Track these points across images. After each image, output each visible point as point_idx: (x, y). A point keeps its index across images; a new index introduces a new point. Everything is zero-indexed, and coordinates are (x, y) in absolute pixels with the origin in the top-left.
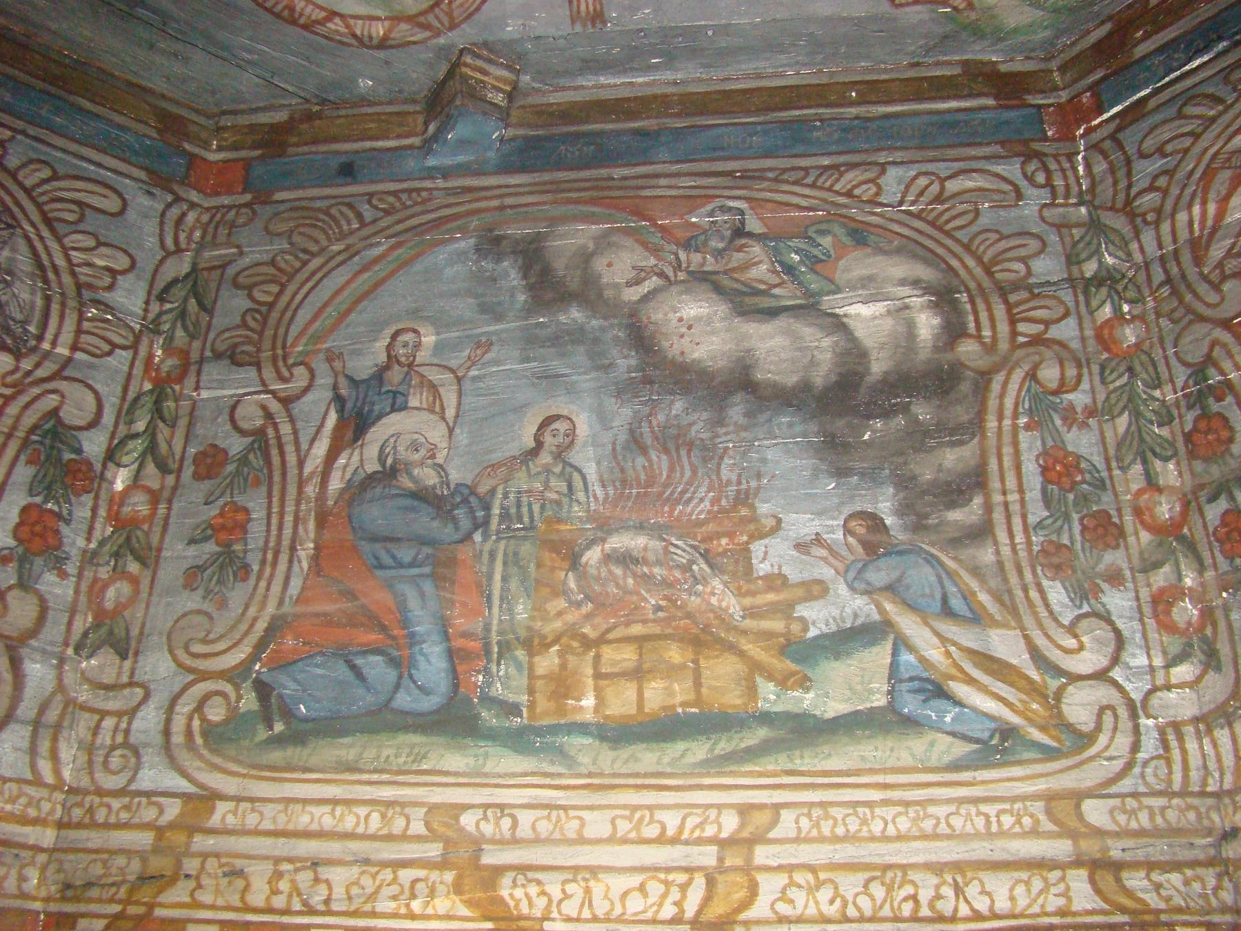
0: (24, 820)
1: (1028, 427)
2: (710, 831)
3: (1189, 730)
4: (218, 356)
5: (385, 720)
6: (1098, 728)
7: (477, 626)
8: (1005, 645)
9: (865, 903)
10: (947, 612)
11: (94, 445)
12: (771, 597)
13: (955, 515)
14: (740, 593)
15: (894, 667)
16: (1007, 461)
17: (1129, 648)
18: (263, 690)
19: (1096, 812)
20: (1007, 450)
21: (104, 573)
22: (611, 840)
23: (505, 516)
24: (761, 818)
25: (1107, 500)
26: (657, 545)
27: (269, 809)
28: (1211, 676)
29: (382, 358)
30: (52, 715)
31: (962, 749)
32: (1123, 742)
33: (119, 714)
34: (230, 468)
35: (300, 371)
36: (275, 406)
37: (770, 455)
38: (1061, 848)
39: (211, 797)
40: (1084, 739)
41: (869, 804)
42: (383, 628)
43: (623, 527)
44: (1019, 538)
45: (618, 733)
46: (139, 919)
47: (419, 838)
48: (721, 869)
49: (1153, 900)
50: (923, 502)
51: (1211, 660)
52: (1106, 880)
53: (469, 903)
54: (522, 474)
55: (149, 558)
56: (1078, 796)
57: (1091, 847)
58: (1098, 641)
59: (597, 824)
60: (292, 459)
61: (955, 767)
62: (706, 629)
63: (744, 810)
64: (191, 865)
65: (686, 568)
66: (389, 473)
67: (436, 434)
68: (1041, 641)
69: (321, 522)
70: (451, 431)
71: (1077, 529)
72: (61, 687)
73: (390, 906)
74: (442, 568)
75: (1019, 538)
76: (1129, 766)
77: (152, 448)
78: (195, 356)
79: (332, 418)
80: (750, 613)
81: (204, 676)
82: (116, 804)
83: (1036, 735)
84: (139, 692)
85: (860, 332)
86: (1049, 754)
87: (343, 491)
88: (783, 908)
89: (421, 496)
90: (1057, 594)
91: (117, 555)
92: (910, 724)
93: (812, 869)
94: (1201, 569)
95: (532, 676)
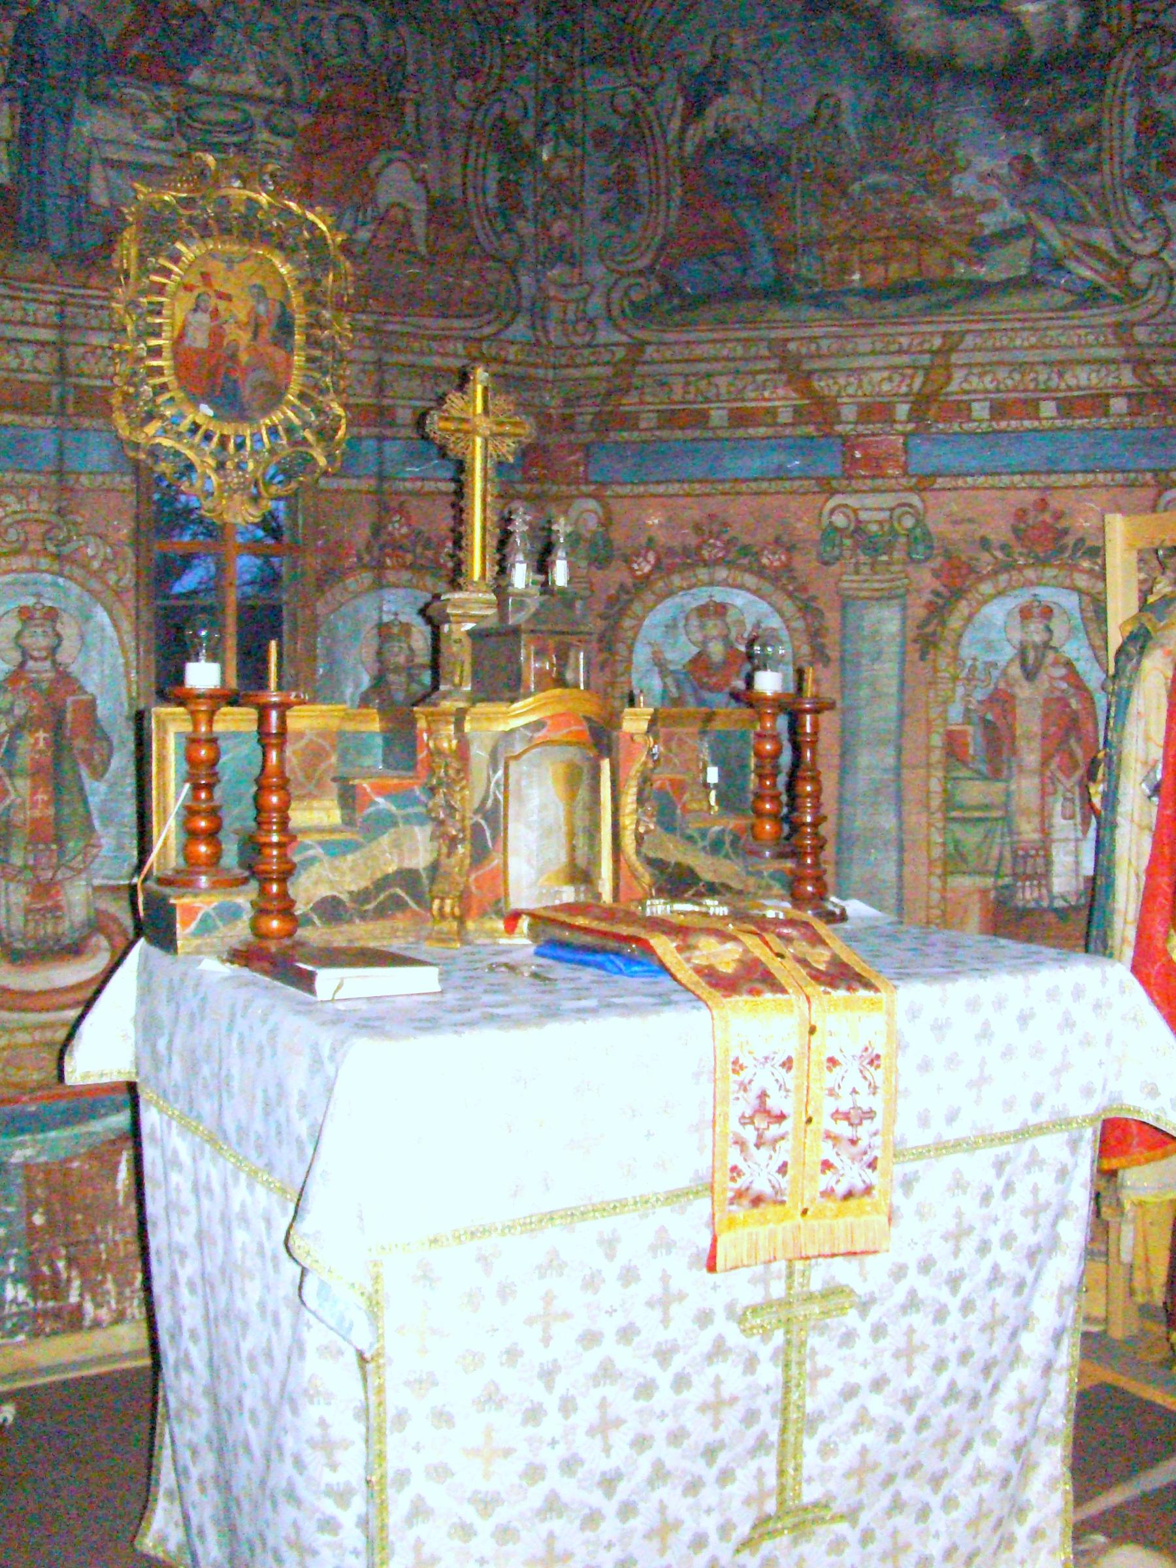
0: (536, 366)
2: (926, 346)
4: (593, 60)
5: (733, 294)
6: (1149, 285)
8: (1100, 238)
10: (1068, 218)
11: (527, 132)
13: (1079, 156)
15: (1034, 251)
18: (665, 282)
19: (1141, 334)
20: (1116, 110)
22: (873, 352)
24: (955, 338)
29: (708, 58)
31: (1068, 298)
32: (1162, 294)
33: (577, 301)
35: (653, 71)
36: (640, 95)
39: (641, 345)
45: (873, 294)
48: (932, 367)
59: (864, 345)
60: (657, 131)
61: (1065, 308)
63: (945, 335)
64: (637, 382)
66: (724, 139)
73: (753, 395)
75: (1117, 171)
76: (1163, 309)
78: (577, 59)
79: (680, 102)
81: (623, 275)
82: (586, 352)
84: (587, 288)
85: (1028, 24)
86: (1119, 301)
88: (966, 386)
89: (746, 152)
90: (1135, 206)
93: (982, 365)
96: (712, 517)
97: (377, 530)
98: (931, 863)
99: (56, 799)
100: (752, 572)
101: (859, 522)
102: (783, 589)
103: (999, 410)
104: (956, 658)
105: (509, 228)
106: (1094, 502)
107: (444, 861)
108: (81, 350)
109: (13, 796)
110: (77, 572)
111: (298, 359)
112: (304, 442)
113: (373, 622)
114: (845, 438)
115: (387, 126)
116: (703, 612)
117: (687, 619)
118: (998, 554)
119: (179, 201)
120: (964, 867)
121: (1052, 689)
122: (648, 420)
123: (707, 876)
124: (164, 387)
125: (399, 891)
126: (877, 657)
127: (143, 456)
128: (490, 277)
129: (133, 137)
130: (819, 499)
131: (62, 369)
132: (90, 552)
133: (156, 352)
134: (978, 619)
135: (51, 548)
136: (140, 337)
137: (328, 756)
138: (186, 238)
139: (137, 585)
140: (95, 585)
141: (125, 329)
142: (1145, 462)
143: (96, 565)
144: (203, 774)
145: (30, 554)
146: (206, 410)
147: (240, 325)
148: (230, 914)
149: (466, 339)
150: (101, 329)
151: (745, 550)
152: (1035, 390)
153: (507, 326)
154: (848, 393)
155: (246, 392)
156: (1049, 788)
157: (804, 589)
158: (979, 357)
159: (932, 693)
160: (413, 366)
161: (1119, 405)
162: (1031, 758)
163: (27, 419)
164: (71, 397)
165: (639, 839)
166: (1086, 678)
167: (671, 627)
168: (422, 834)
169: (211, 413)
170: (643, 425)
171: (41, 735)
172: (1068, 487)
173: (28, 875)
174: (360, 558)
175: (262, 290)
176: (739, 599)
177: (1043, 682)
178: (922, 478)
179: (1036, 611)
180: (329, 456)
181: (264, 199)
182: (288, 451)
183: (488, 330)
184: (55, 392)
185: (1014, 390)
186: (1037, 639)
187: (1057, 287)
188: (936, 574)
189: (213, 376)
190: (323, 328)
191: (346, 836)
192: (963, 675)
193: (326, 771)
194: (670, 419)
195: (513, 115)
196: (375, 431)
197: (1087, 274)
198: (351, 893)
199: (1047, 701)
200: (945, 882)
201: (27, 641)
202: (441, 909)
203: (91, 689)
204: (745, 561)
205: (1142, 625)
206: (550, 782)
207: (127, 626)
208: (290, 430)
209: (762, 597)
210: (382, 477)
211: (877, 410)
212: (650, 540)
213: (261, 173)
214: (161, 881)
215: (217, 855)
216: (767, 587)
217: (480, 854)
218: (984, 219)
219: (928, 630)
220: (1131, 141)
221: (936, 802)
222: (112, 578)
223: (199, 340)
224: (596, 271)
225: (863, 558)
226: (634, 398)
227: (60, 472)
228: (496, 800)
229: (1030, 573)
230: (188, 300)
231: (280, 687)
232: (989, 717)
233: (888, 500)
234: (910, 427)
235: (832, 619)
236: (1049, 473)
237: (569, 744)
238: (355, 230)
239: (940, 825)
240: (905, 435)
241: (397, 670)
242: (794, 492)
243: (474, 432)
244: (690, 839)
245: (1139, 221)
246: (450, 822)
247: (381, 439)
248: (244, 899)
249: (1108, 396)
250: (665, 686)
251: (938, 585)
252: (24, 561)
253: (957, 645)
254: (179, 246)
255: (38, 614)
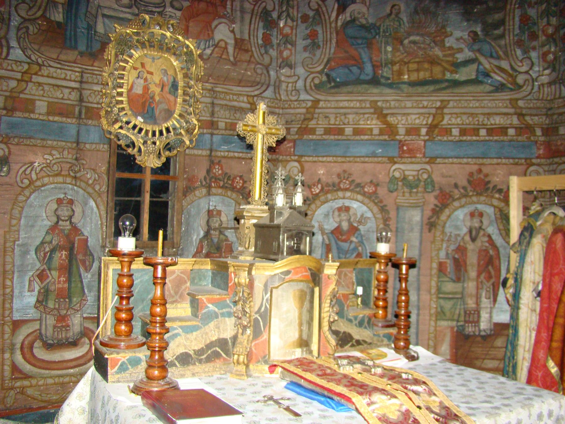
0: (275, 108)
1: (518, 8)
2: (434, 106)
3: (546, 86)
5: (358, 82)
6: (524, 85)
7: (379, 59)
8: (505, 64)
9: (467, 121)
10: (491, 56)
12: (449, 52)
14: (442, 51)
15: (477, 70)
16: (511, 17)
17: (535, 66)
18: (328, 75)
19: (521, 103)
20: (511, 14)
21: (282, 48)
22: (412, 107)
23: (384, 32)
24: (446, 103)
25: (535, 28)
26: (422, 39)
27: (333, 103)
28: (554, 73)
30: (277, 84)
31: (492, 88)
32: (530, 88)
33: (293, 83)
34: (311, 20)
37: (450, 15)
38: (512, 111)
39: (318, 101)
40: (520, 87)
41: (470, 100)
42: (356, 60)
43: (413, 35)
44: (511, 38)
45: (412, 84)
46: (305, 128)
47: (368, 108)
48: (436, 114)
49: (531, 122)
50: (488, 28)
51: (554, 70)
52: (521, 118)
53: (381, 122)
54: (387, 20)
55: (293, 44)
56: (517, 100)
57: (518, 111)
58: (527, 64)
59: (409, 104)
60: (327, 17)
61: (490, 92)
62: (434, 60)
63: (442, 101)
65: (429, 45)
67: (364, 10)
68: (513, 64)
69: (337, 34)
70: (368, 9)
71: (526, 36)
72: (278, 77)
74: (369, 45)
75: (511, 38)
76: (530, 93)
77: (288, 15)
79: (336, 6)
80: (445, 56)
81: (312, 73)
82: (296, 103)
83: (509, 86)
86: (511, 90)
87: (342, 25)
88: (450, 122)
89: (362, 26)
90: (519, 52)
91: (284, 43)
92: (481, 83)
94: (556, 46)
95: (393, 71)
96: (345, 171)
97: (208, 172)
98: (431, 315)
99: (69, 281)
100: (361, 194)
101: (404, 175)
102: (373, 201)
103: (463, 132)
104: (443, 232)
105: (266, 52)
106: (501, 171)
107: (239, 336)
108: (89, 92)
109: (50, 278)
110: (83, 185)
111: (179, 100)
112: (181, 134)
113: (205, 210)
114: (400, 141)
115: (219, 9)
116: (340, 209)
117: (333, 212)
118: (462, 191)
119: (133, 33)
120: (444, 318)
121: (482, 246)
122: (320, 131)
123: (356, 337)
124: (123, 109)
125: (218, 349)
126: (412, 230)
127: (113, 137)
128: (259, 71)
129: (116, 6)
130: (389, 165)
131: (81, 100)
132: (89, 176)
133: (120, 94)
134: (453, 216)
135: (72, 174)
136: (114, 88)
137: (186, 282)
138: (136, 48)
139: (108, 191)
140: (90, 190)
141: (108, 84)
142: (523, 156)
143: (91, 182)
144: (125, 292)
145: (63, 176)
146: (140, 119)
147: (156, 85)
148: (135, 362)
149: (248, 96)
150: (97, 84)
151: (358, 185)
152: (478, 125)
153: (264, 91)
154: (401, 124)
155: (157, 113)
156: (480, 286)
157: (381, 201)
158: (455, 111)
159: (433, 246)
160: (226, 105)
161: (511, 132)
162: (473, 274)
163: (64, 119)
164: (84, 111)
165: (331, 323)
166: (495, 242)
167: (327, 215)
168: (230, 322)
169: (142, 120)
170: (317, 133)
171: (64, 252)
172: (490, 164)
173: (56, 312)
174: (201, 182)
175: (166, 71)
176: (355, 205)
177: (478, 243)
178: (431, 158)
179: (476, 214)
180: (191, 141)
181: (168, 34)
182: (174, 137)
183: (256, 93)
184: (77, 109)
185: (469, 125)
186: (477, 225)
187: (487, 83)
188: (436, 198)
189: (144, 105)
190: (190, 88)
191: (194, 323)
192: (446, 239)
193: (185, 290)
194: (328, 131)
195: (270, 8)
196: (210, 131)
197: (499, 79)
198: (194, 350)
199: (480, 251)
200: (436, 323)
201: (59, 213)
202: (238, 360)
203: (86, 234)
204: (358, 189)
205: (529, 223)
206: (292, 299)
207: (102, 208)
208: (175, 129)
209: (364, 204)
210: (211, 150)
211: (413, 131)
212: (319, 180)
213: (168, 24)
214: (102, 344)
215: (131, 331)
216: (366, 201)
217: (257, 333)
218: (458, 56)
219: (432, 220)
220: (516, 27)
221: (433, 291)
222: (97, 188)
223: (139, 90)
224: (300, 71)
225: (406, 190)
226: (314, 122)
227: (78, 143)
228: (266, 307)
229: (474, 199)
230: (135, 73)
231: (163, 254)
232: (456, 256)
233: (417, 167)
234: (427, 138)
235: (393, 214)
236: (483, 158)
237: (301, 281)
238: (205, 49)
239: (435, 300)
240: (425, 141)
241: (215, 229)
242: (379, 163)
243: (259, 131)
244: (350, 321)
245: (520, 58)
246: (243, 318)
247: (212, 134)
248: (143, 354)
249: (507, 128)
250: (323, 239)
251: (436, 202)
252: (60, 179)
253: (444, 227)
254: (132, 51)
255: (65, 202)
